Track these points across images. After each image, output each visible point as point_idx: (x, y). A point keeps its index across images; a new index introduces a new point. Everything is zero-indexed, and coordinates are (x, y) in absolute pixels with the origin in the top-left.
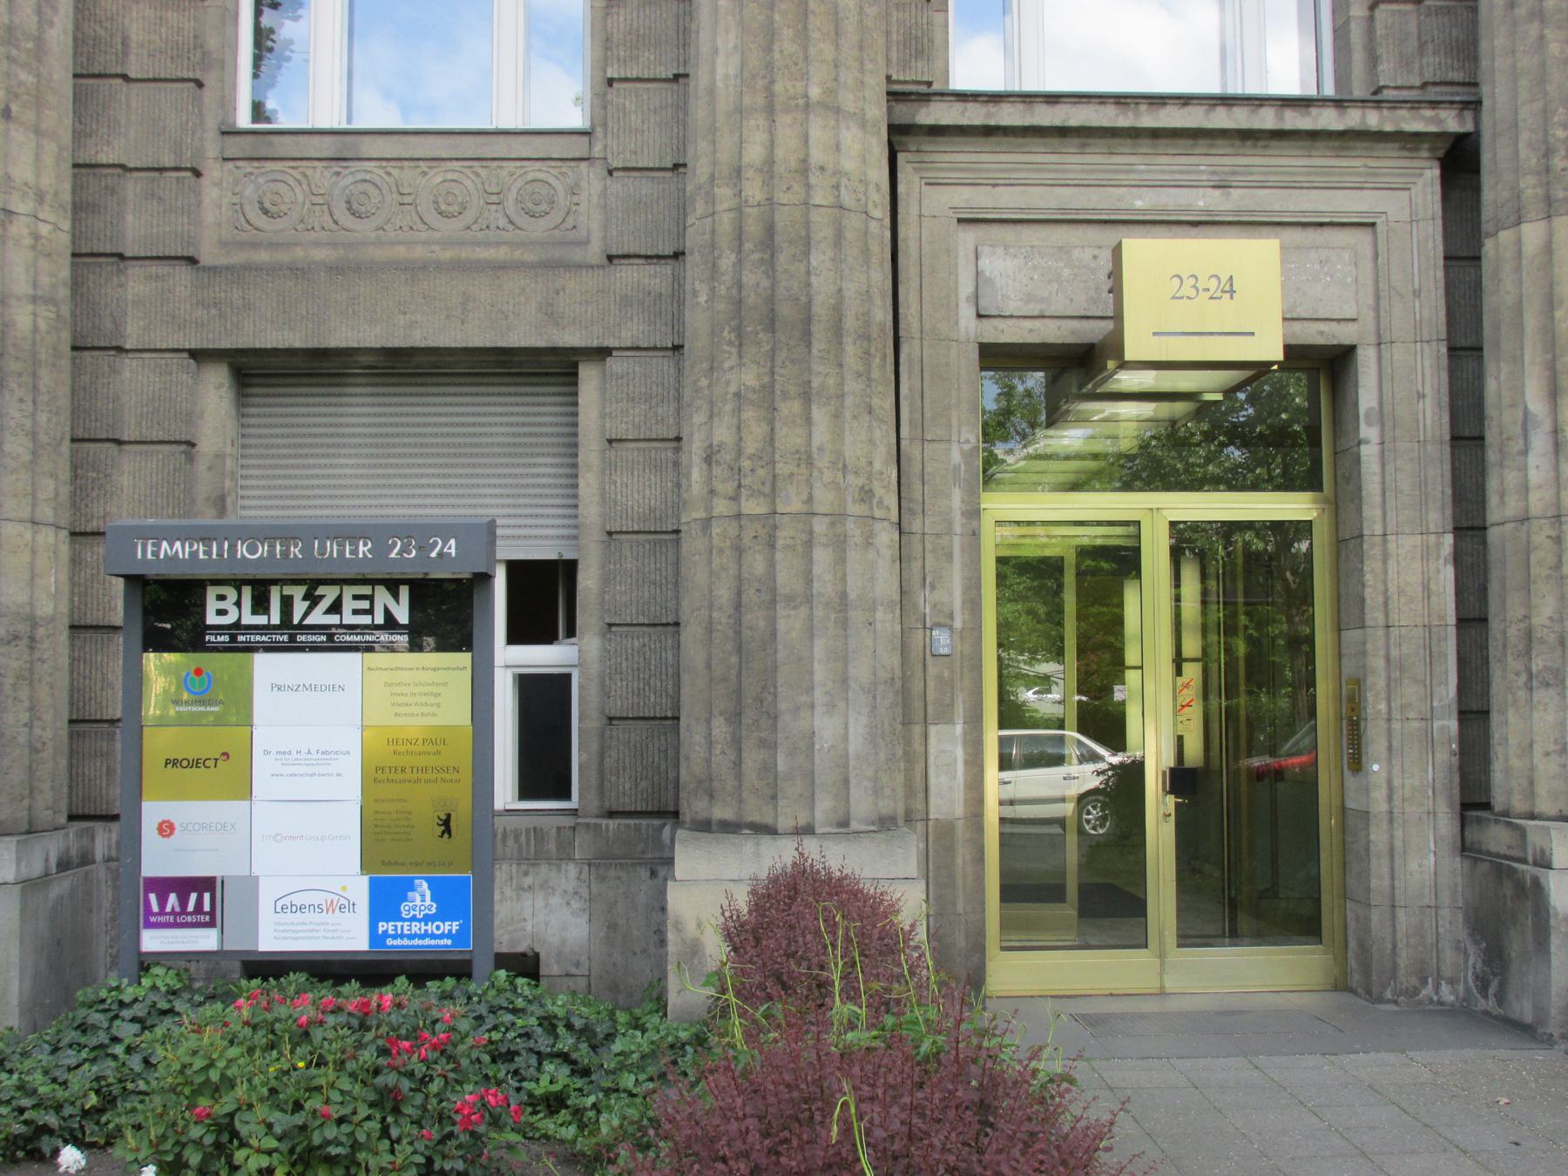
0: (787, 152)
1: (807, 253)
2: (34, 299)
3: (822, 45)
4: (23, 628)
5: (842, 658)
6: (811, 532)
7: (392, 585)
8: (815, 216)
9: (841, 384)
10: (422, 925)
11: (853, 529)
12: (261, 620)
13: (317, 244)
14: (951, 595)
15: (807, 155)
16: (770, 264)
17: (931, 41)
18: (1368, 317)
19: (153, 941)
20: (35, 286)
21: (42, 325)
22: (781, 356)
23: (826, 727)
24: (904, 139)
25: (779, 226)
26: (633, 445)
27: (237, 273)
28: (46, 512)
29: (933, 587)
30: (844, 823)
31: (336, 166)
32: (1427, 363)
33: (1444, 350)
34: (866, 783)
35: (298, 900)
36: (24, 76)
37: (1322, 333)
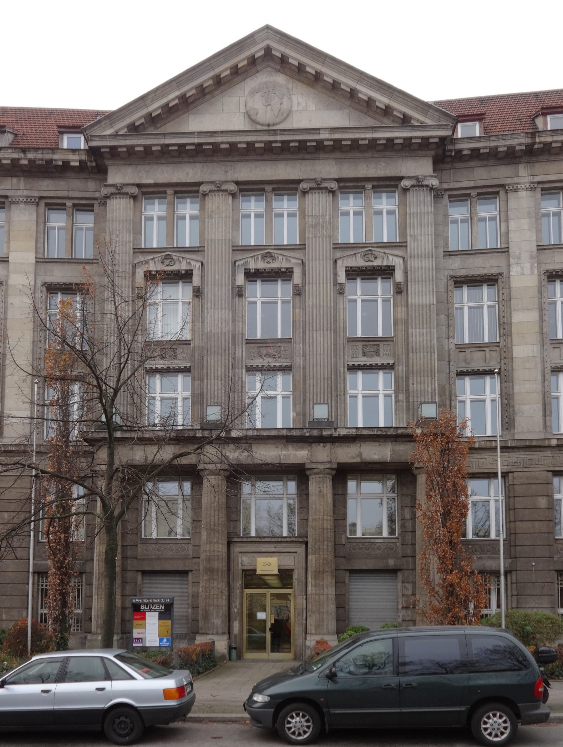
7: (162, 605)
11: (220, 597)
19: (134, 645)
30: (217, 633)
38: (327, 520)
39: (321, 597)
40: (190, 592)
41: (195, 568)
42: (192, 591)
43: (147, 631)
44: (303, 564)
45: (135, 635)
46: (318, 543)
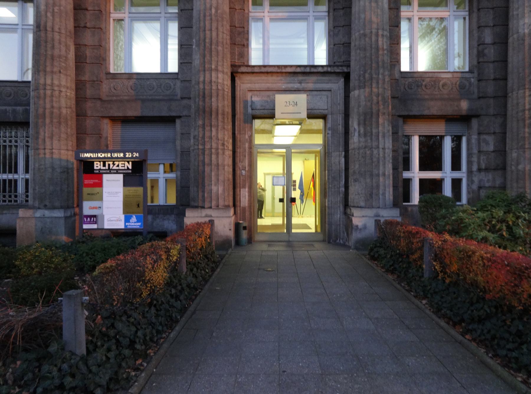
0: (207, 79)
1: (211, 99)
2: (66, 108)
4: (65, 170)
5: (217, 175)
8: (213, 91)
10: (135, 224)
11: (220, 151)
12: (104, 168)
13: (125, 96)
16: (204, 101)
18: (330, 109)
19: (85, 226)
20: (67, 105)
21: (69, 112)
23: (214, 188)
27: (110, 102)
28: (70, 148)
30: (218, 206)
31: (129, 80)
35: (112, 219)
36: (63, 64)
39: (375, 152)
40: (179, 148)
41: (184, 113)
42: (181, 146)
43: (104, 202)
44: (341, 107)
45: (87, 211)
46: (369, 71)
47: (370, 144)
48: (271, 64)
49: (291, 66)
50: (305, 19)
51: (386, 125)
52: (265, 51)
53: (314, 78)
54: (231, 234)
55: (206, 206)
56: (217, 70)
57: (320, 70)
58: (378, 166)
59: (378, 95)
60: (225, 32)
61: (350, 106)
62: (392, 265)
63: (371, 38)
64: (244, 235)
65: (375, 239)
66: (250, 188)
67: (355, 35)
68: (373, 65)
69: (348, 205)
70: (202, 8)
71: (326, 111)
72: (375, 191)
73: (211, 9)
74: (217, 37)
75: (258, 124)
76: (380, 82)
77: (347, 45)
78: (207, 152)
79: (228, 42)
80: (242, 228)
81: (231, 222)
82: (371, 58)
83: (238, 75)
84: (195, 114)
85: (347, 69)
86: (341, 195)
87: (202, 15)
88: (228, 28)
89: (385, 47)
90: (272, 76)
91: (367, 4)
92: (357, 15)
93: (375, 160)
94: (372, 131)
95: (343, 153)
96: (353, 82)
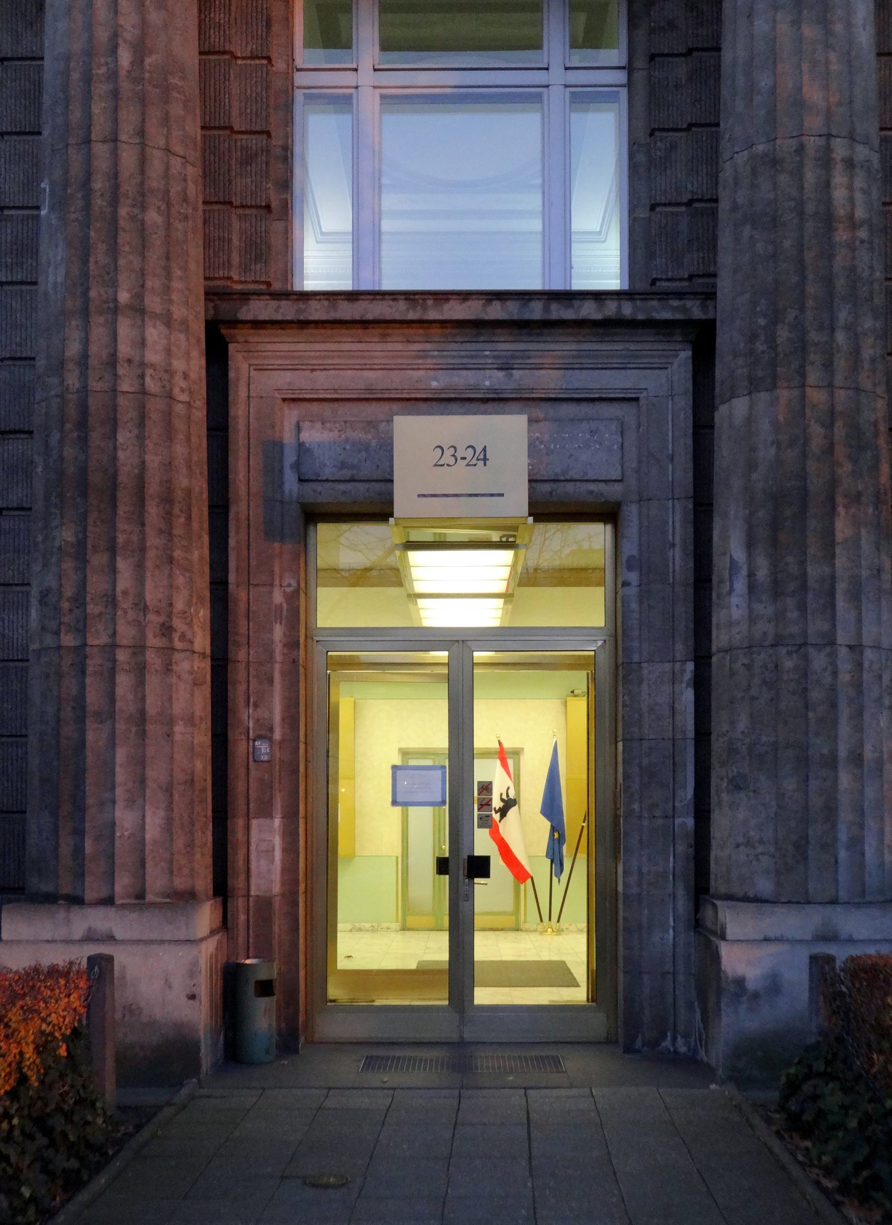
0: (98, 350)
1: (114, 431)
3: (131, 257)
5: (140, 762)
6: (115, 661)
8: (121, 401)
9: (143, 540)
11: (151, 657)
14: (271, 712)
15: (116, 351)
16: (83, 441)
17: (269, 247)
22: (92, 517)
24: (232, 331)
25: (92, 409)
26: (18, 588)
29: (256, 706)
30: (141, 896)
32: (678, 517)
33: (691, 506)
34: (163, 864)
37: (591, 492)
38: (850, 164)
39: (819, 660)
44: (681, 471)
47: (795, 629)
48: (387, 285)
49: (465, 296)
50: (528, 98)
51: (866, 546)
52: (365, 238)
53: (564, 347)
54: (199, 1015)
55: (90, 895)
56: (139, 310)
57: (588, 311)
58: (830, 722)
59: (831, 417)
60: (178, 149)
61: (717, 463)
62: (866, 1164)
63: (798, 174)
64: (262, 1017)
65: (812, 1040)
66: (291, 816)
67: (735, 162)
68: (811, 289)
69: (706, 890)
70: (77, 46)
71: (618, 487)
72: (815, 831)
73: (114, 50)
74: (143, 172)
75: (341, 545)
76: (841, 363)
77: (704, 207)
78: (93, 663)
79: (193, 190)
80: (251, 989)
81: (195, 963)
82: (801, 262)
83: (241, 334)
84: (47, 497)
85: (704, 307)
86: (681, 848)
87: (75, 76)
88: (194, 129)
89: (860, 213)
90: (384, 337)
91: (784, 28)
92: (741, 80)
93: (816, 695)
94: (805, 574)
95: (690, 666)
96: (728, 363)
